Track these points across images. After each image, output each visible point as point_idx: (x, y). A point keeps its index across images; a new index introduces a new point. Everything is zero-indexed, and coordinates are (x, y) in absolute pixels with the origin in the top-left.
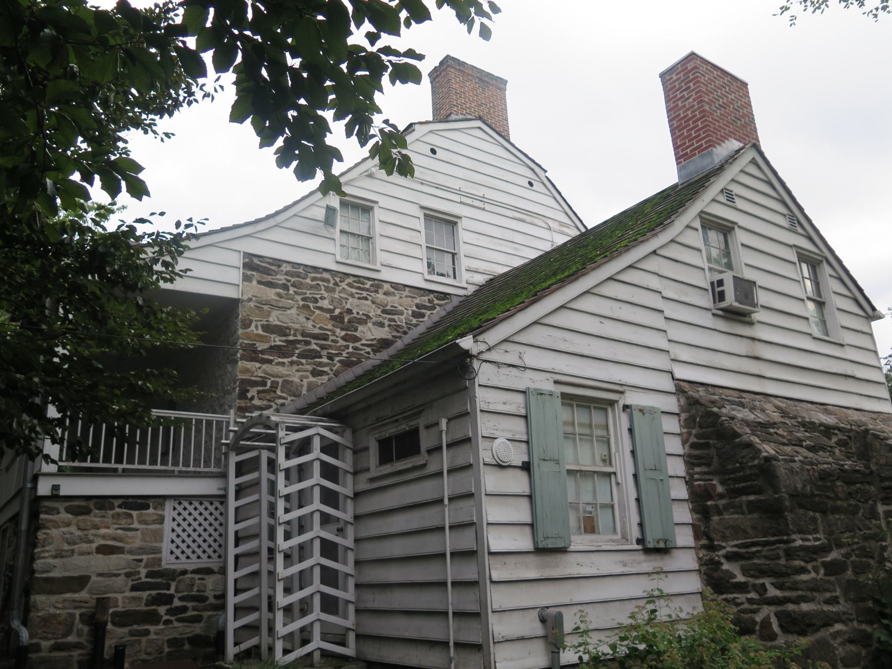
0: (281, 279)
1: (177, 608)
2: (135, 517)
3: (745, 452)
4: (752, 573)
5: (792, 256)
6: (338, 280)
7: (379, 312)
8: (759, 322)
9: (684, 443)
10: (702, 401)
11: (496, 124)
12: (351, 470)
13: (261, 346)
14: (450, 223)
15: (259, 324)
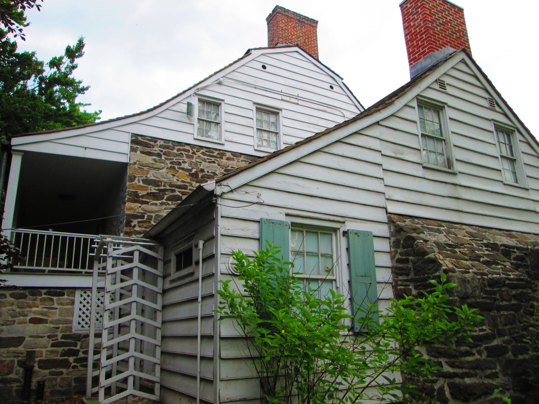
0: (157, 150)
1: (81, 358)
2: (55, 301)
3: (431, 266)
4: (433, 353)
5: (491, 127)
6: (195, 150)
7: (223, 171)
8: (460, 172)
9: (392, 258)
10: (405, 229)
11: (310, 49)
12: (161, 275)
13: (141, 193)
14: (274, 112)
15: (141, 179)
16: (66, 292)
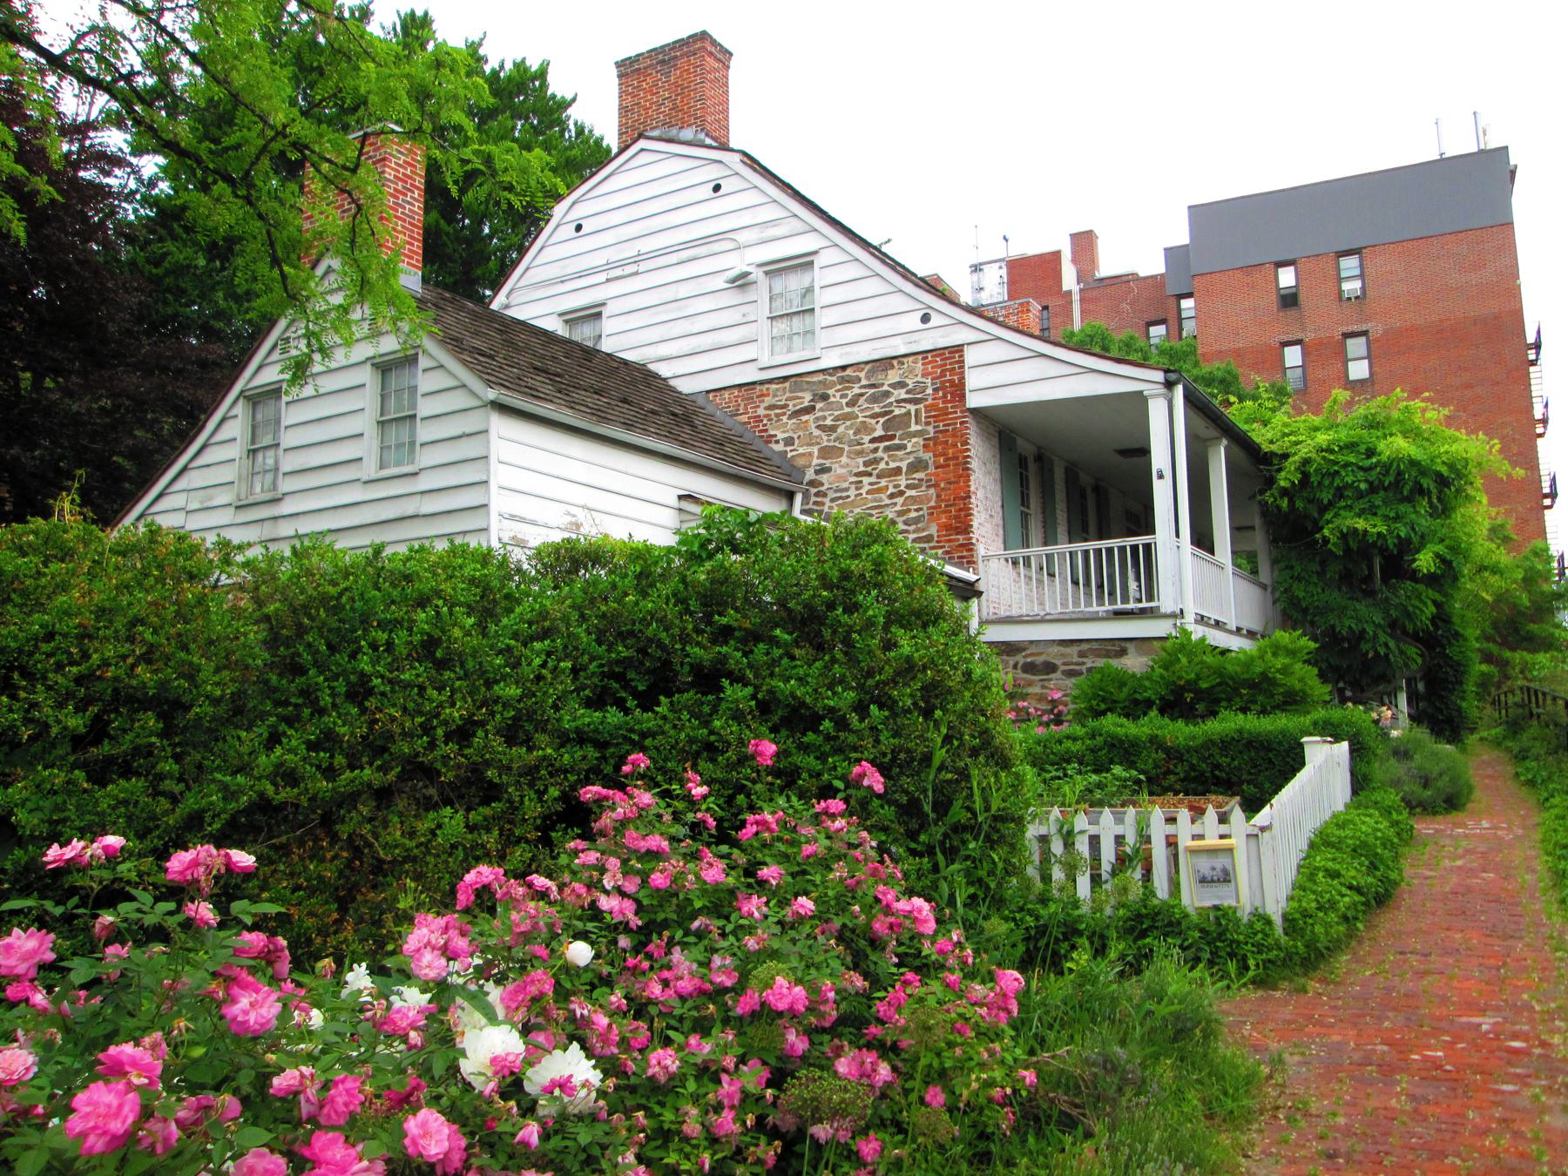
16: (1131, 647)
